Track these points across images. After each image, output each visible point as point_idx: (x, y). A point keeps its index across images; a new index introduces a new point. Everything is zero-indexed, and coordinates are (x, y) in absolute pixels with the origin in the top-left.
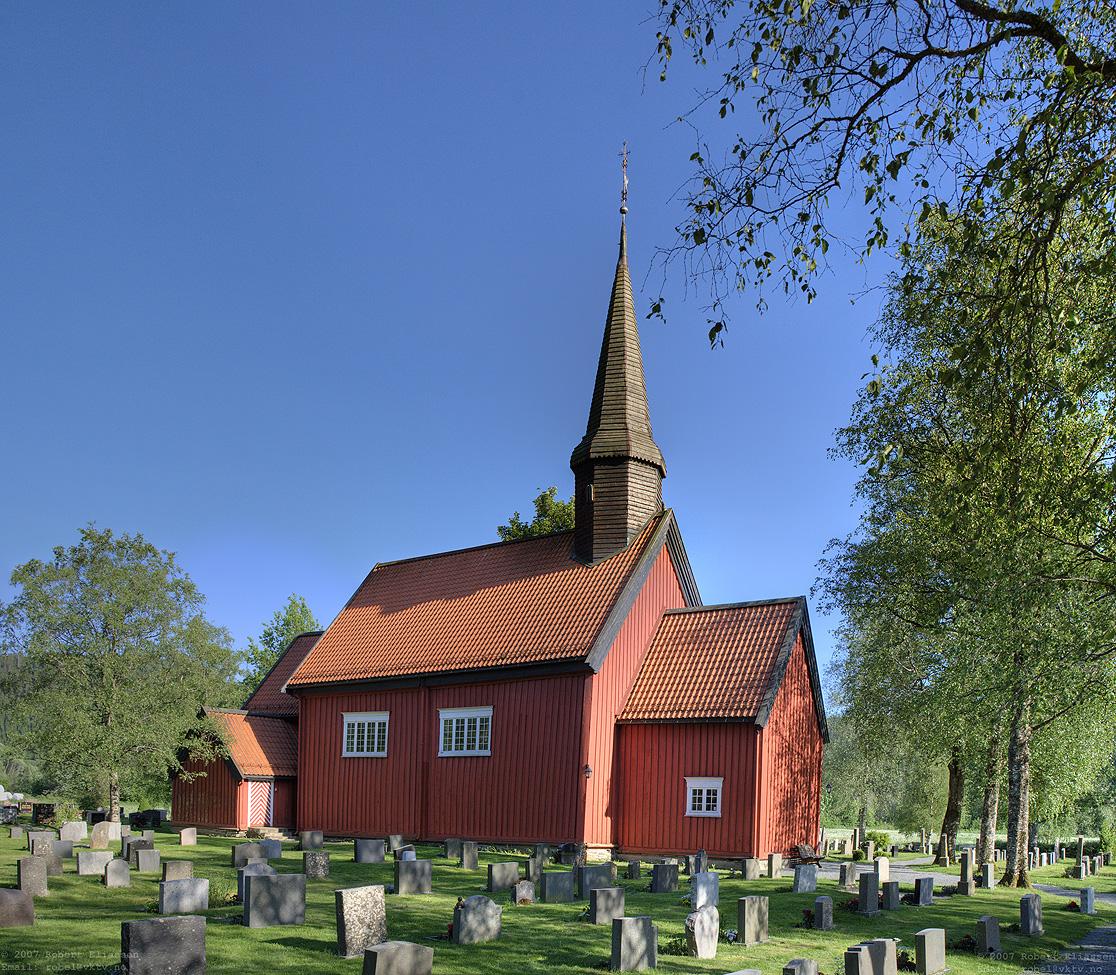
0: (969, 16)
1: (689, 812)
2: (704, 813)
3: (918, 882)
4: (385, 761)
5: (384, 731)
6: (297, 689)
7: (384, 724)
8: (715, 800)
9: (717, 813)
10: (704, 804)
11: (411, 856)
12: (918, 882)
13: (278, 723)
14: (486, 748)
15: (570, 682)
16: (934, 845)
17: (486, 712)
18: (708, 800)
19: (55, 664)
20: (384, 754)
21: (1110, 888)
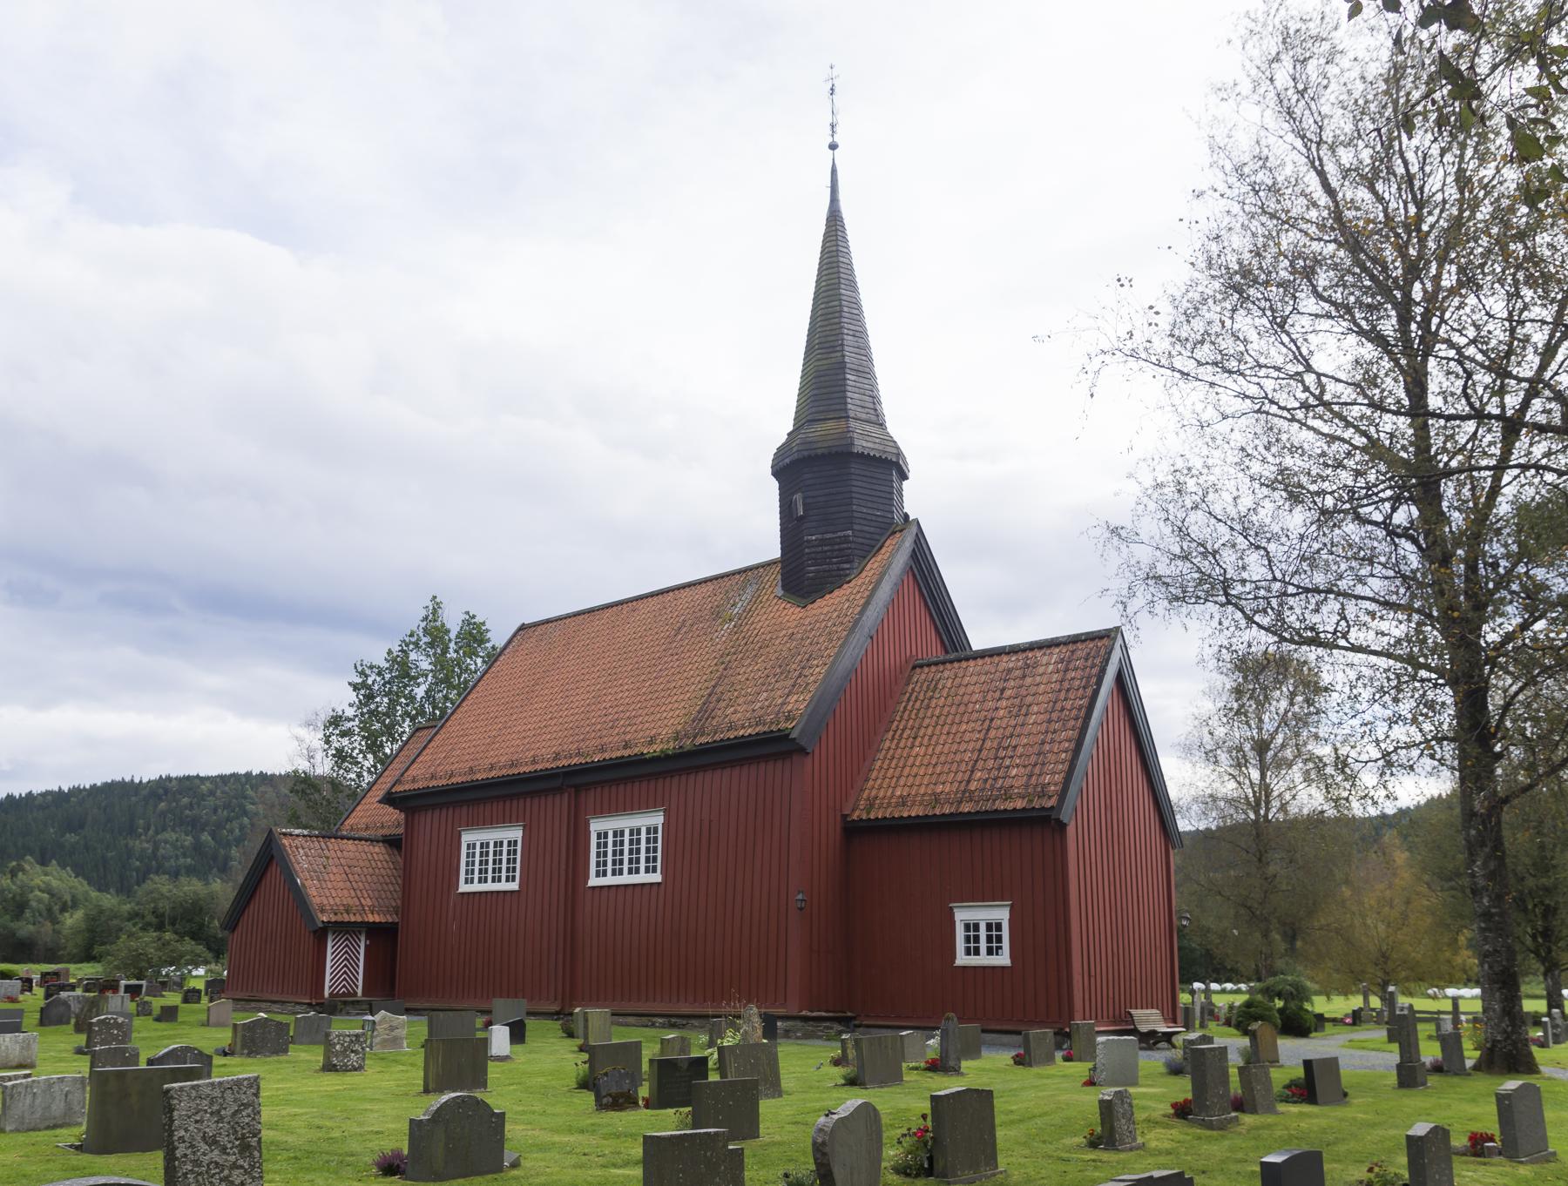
0: (1363, 339)
1: (962, 959)
2: (983, 960)
3: (1308, 1064)
4: (663, 887)
5: (655, 840)
6: (400, 797)
7: (516, 842)
8: (999, 939)
9: (1003, 959)
10: (983, 945)
11: (1214, 986)
12: (1308, 1064)
13: (378, 849)
14: (654, 870)
15: (501, 806)
16: (643, 1099)
17: (516, 834)
18: (989, 939)
19: (1249, 653)
20: (514, 886)
21: (839, 1174)
